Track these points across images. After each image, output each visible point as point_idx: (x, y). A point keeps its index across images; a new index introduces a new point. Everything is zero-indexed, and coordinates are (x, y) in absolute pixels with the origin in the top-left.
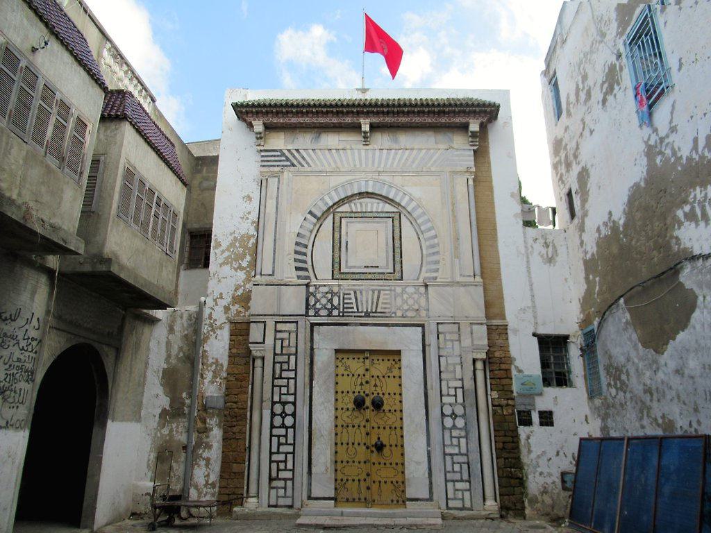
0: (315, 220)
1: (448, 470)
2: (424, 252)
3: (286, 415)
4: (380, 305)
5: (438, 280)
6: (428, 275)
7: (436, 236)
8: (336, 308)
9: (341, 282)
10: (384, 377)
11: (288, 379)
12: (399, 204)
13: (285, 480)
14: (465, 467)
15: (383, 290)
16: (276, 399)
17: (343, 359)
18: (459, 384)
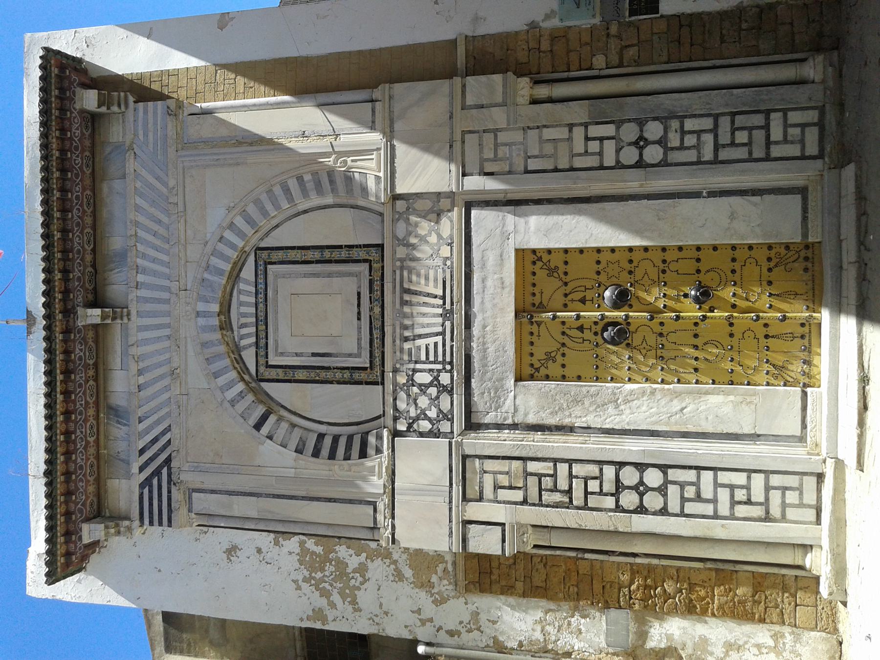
0: (272, 419)
1: (746, 156)
2: (329, 200)
7: (300, 179)
8: (436, 378)
9: (388, 366)
10: (566, 284)
11: (571, 476)
12: (243, 251)
13: (768, 488)
14: (740, 120)
16: (610, 502)
17: (532, 365)
18: (578, 132)
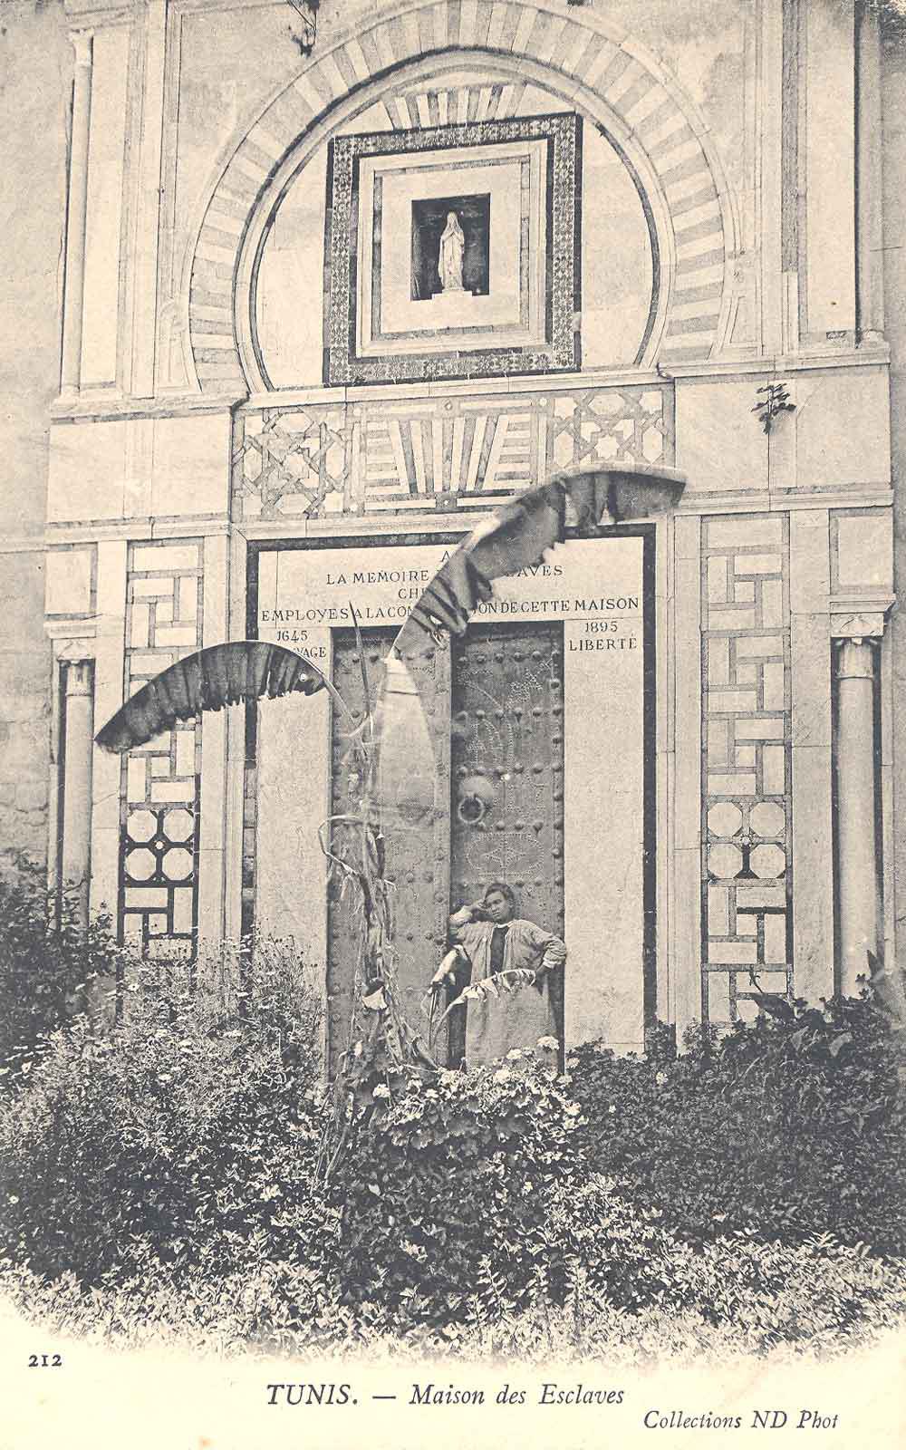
3: (169, 845)
4: (495, 468)
5: (718, 357)
6: (670, 343)
15: (399, 498)
